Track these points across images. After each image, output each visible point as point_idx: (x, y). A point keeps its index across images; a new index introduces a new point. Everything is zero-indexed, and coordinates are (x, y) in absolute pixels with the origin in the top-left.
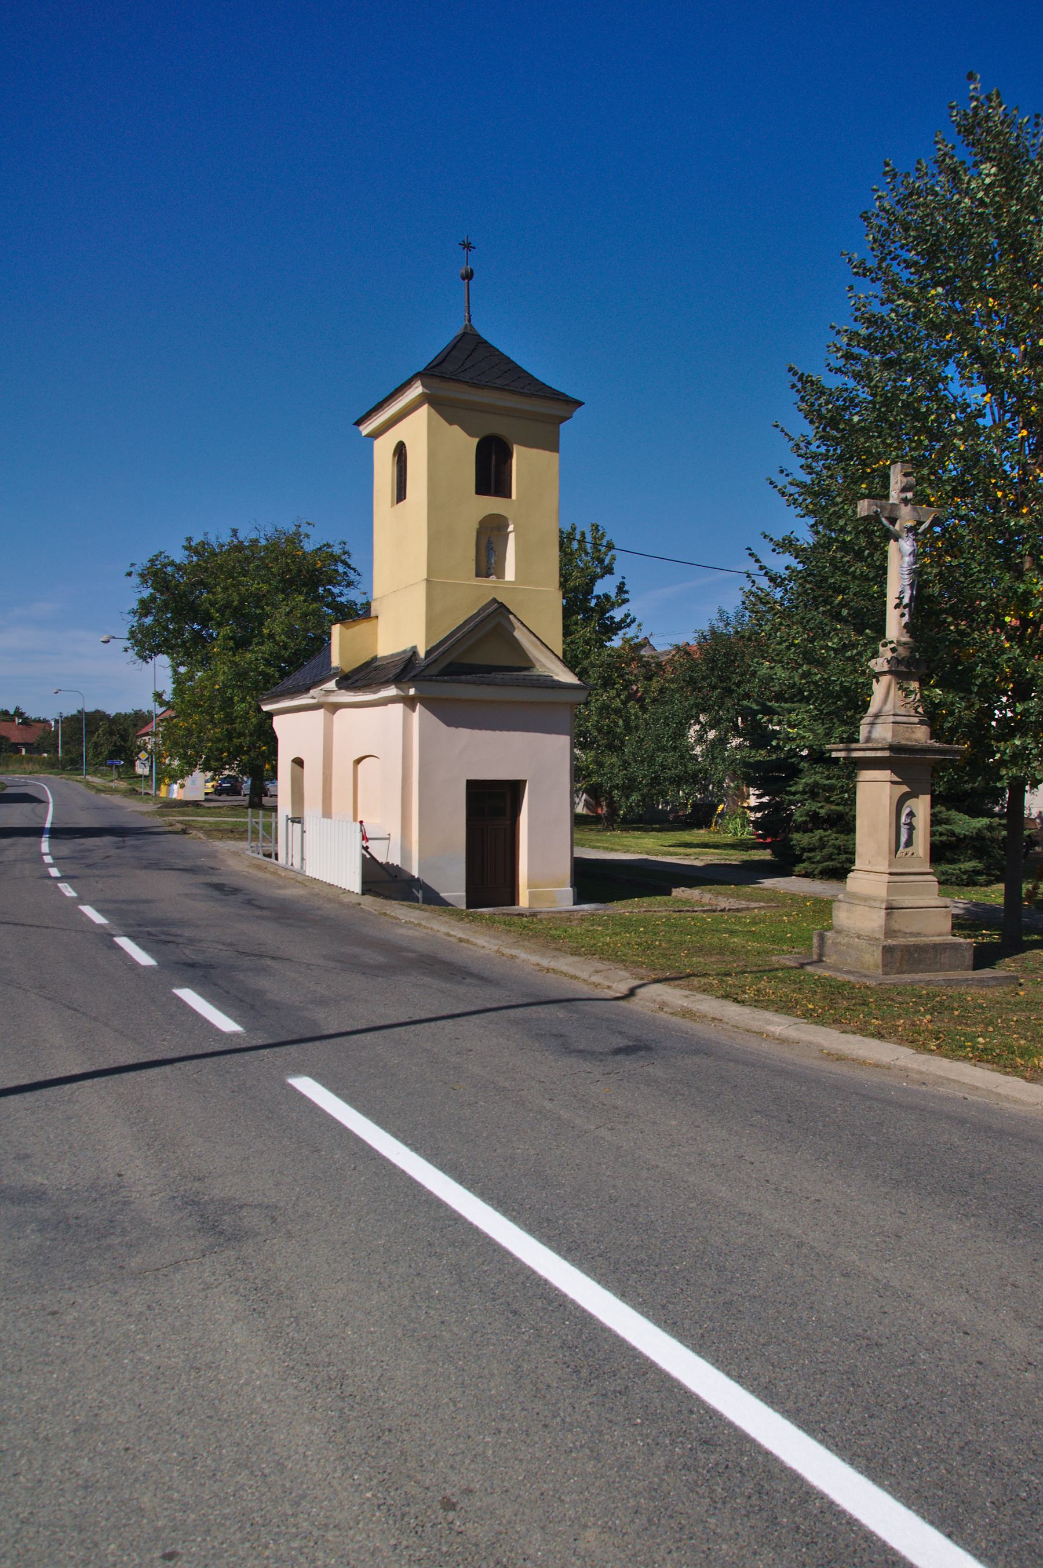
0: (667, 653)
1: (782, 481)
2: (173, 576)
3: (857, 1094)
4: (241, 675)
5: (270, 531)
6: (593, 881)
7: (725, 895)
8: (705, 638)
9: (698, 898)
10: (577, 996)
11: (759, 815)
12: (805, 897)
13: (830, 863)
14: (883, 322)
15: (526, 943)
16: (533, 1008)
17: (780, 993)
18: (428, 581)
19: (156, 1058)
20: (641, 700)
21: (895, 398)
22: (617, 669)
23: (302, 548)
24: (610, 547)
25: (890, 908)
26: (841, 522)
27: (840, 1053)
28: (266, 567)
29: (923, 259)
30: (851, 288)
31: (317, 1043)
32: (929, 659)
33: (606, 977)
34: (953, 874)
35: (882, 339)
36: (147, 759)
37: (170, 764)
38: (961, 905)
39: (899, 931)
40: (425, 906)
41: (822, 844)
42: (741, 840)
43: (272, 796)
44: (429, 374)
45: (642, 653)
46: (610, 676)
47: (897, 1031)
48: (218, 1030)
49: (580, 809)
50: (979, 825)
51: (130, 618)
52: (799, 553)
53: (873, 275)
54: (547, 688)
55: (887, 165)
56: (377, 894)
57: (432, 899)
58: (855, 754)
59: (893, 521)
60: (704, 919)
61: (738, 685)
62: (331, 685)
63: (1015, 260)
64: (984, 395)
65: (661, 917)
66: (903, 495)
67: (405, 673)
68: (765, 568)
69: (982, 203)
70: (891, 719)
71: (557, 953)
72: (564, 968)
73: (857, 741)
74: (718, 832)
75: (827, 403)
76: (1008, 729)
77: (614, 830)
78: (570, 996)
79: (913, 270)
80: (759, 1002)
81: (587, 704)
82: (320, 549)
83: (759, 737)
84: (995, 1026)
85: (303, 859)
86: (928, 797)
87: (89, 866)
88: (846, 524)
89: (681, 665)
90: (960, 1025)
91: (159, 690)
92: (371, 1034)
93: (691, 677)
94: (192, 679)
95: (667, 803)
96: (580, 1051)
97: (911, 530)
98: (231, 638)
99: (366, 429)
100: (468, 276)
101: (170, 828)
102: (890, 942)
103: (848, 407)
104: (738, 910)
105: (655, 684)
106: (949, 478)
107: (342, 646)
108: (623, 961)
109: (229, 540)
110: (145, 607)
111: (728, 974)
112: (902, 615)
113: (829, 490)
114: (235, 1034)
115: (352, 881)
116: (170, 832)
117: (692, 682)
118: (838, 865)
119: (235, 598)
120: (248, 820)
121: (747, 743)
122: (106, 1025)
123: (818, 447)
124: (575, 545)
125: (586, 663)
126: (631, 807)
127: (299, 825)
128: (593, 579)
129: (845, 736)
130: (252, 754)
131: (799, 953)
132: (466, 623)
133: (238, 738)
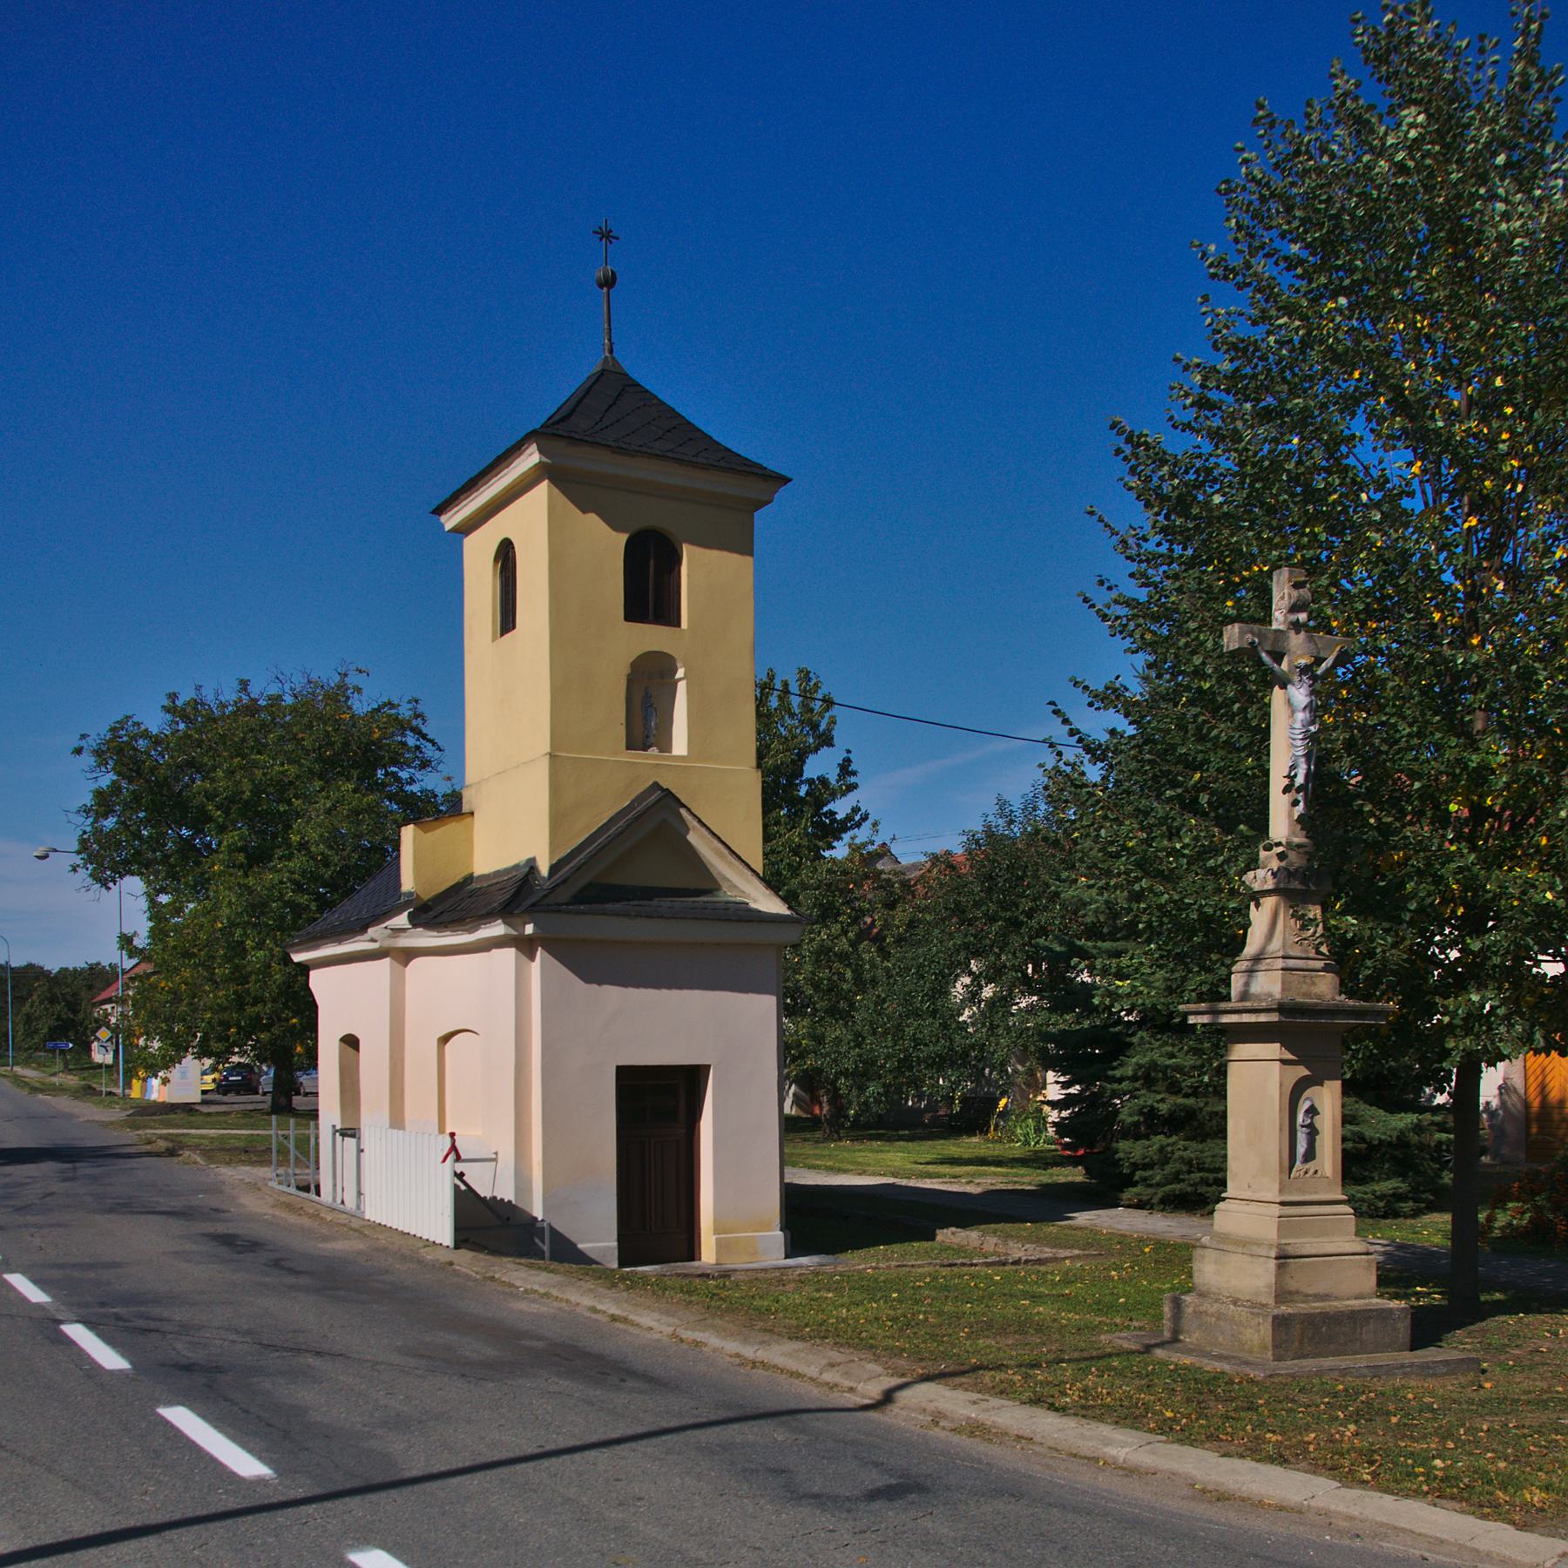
0: (915, 866)
1: (1102, 597)
2: (148, 753)
3: (1256, 1556)
4: (258, 908)
5: (299, 682)
6: (812, 1220)
7: (1019, 1238)
8: (977, 842)
9: (977, 1244)
10: (802, 1406)
11: (1065, 1114)
12: (1141, 1240)
13: (1176, 1187)
14: (1257, 349)
15: (718, 1321)
16: (736, 1426)
17: (1118, 1394)
18: (552, 757)
19: (132, 1523)
20: (878, 939)
21: (1277, 467)
22: (842, 891)
23: (350, 708)
24: (829, 702)
25: (1283, 1257)
26: (1197, 660)
27: (1222, 1489)
28: (295, 738)
29: (1314, 255)
30: (1206, 299)
31: (394, 1493)
32: (1338, 868)
33: (847, 1374)
34: (1363, 1200)
35: (1254, 377)
36: (110, 1039)
37: (147, 1047)
38: (1379, 1248)
39: (1297, 1292)
40: (555, 1265)
41: (1164, 1158)
42: (1036, 1152)
43: (306, 1094)
44: (548, 434)
45: (880, 866)
46: (831, 903)
47: (1306, 1451)
48: (233, 1474)
49: (788, 1108)
50: (1401, 1125)
51: (80, 819)
52: (1130, 709)
53: (1239, 278)
54: (740, 921)
55: (1261, 107)
56: (477, 1247)
57: (565, 1253)
58: (1226, 1019)
59: (1278, 657)
60: (989, 1277)
61: (1030, 914)
62: (402, 920)
63: (1455, 257)
64: (1410, 464)
65: (922, 1277)
66: (1293, 617)
67: (516, 901)
68: (1078, 732)
69: (1401, 169)
70: (1280, 963)
71: (767, 1337)
72: (780, 1361)
73: (1227, 998)
74: (1000, 1141)
75: (1173, 475)
76: (1458, 981)
77: (840, 1139)
78: (793, 1405)
79: (1299, 271)
80: (1088, 1410)
81: (796, 947)
82: (378, 710)
83: (1067, 997)
84: (1457, 1440)
85: (359, 1193)
86: (1338, 1084)
87: (19, 1210)
88: (1204, 663)
89: (941, 885)
90: (1402, 1439)
91: (128, 931)
92: (479, 1476)
93: (957, 903)
94: (178, 911)
95: (920, 1097)
96: (816, 1496)
97: (1305, 670)
98: (240, 850)
99: (450, 520)
100: (609, 282)
101: (148, 1148)
102: (1284, 1309)
103: (1202, 484)
104: (1040, 1262)
105: (901, 915)
106: (1361, 591)
107: (417, 859)
108: (872, 1347)
109: (235, 697)
110: (104, 802)
111: (1035, 1365)
112: (1295, 803)
113: (1176, 611)
114: (260, 1481)
115: (438, 1226)
116: (149, 1154)
117: (958, 910)
118: (1189, 1189)
119: (247, 787)
120: (271, 1132)
121: (1045, 1004)
122: (50, 1470)
123: (1159, 544)
124: (774, 702)
125: (794, 882)
126: (866, 1103)
127: (354, 1141)
128: (802, 757)
129: (1205, 988)
130: (276, 1030)
131: (1140, 1328)
132: (612, 821)
133: (254, 1005)
